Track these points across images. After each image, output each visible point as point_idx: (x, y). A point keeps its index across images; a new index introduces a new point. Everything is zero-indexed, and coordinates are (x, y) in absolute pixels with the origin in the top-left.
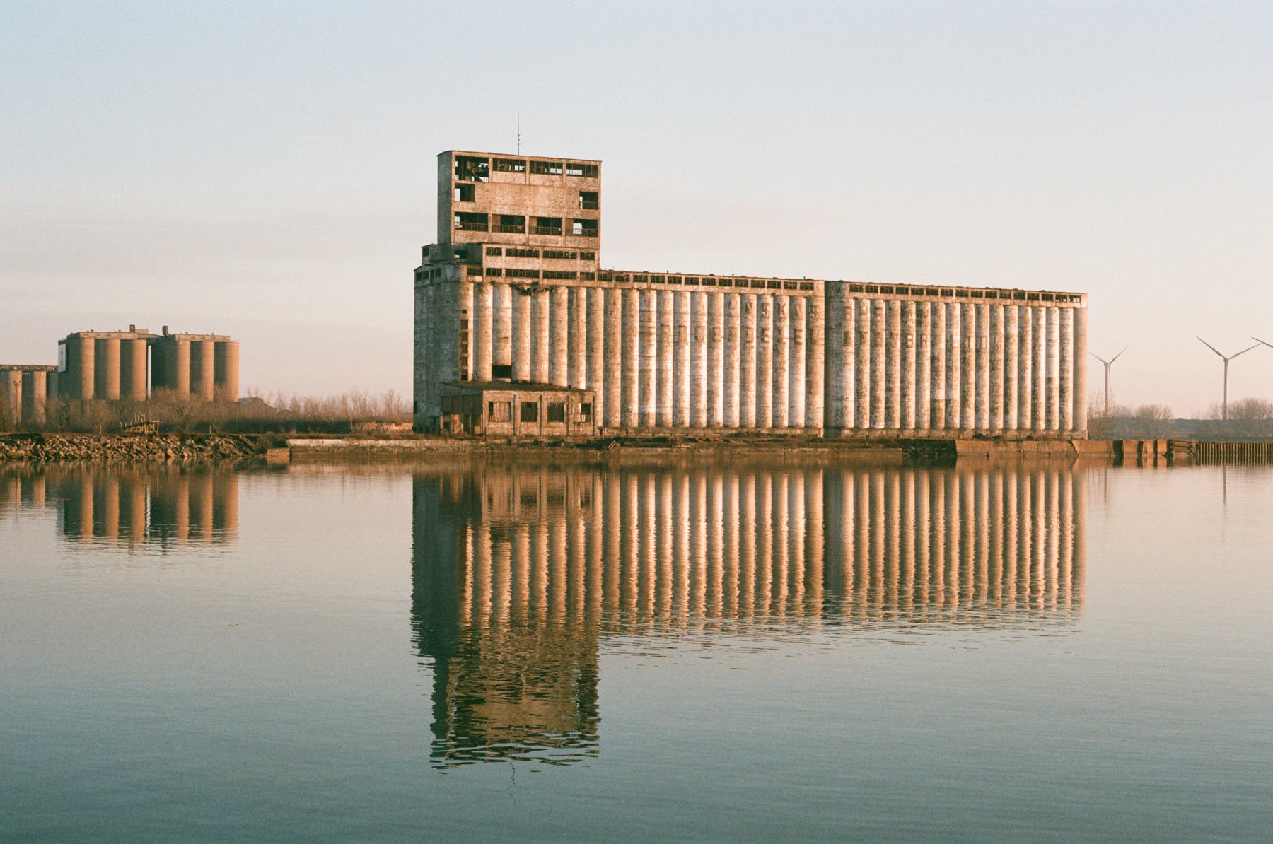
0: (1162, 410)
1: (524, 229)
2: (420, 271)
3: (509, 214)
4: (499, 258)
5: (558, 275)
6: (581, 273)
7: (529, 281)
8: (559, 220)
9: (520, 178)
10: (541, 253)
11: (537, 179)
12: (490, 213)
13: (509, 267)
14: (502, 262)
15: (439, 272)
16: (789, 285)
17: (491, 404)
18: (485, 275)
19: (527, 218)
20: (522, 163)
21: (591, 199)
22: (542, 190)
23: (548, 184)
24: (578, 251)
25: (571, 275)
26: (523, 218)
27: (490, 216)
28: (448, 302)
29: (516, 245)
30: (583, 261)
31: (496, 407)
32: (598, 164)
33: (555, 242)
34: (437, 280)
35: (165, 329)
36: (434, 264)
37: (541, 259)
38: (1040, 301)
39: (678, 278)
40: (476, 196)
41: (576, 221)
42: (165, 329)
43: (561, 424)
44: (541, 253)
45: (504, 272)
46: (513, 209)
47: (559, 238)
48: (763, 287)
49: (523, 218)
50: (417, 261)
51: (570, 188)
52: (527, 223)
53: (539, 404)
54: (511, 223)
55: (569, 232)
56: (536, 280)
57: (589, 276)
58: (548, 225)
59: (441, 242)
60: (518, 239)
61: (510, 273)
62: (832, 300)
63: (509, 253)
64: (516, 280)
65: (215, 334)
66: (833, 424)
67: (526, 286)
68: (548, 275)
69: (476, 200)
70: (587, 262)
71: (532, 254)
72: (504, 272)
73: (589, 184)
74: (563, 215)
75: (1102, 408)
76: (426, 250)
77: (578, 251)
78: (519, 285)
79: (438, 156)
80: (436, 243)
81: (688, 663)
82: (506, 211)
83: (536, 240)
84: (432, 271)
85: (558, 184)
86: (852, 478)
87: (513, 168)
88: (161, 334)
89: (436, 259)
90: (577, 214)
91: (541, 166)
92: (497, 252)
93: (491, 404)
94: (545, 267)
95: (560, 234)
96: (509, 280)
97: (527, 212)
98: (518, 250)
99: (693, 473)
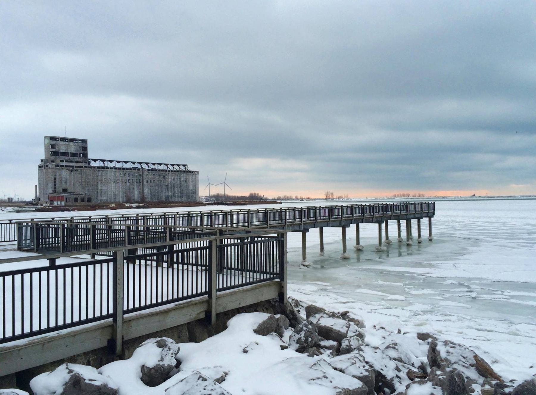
0: (287, 196)
2: (40, 165)
4: (63, 163)
6: (84, 166)
7: (71, 168)
8: (77, 153)
9: (67, 143)
10: (74, 162)
11: (71, 143)
12: (60, 152)
13: (66, 165)
14: (64, 164)
15: (47, 166)
17: (66, 198)
18: (60, 167)
19: (69, 153)
20: (68, 139)
22: (73, 146)
23: (74, 145)
24: (83, 161)
25: (82, 167)
26: (68, 153)
31: (68, 199)
33: (77, 159)
37: (74, 163)
41: (81, 154)
43: (84, 202)
44: (74, 162)
45: (65, 166)
47: (78, 158)
48: (128, 170)
49: (68, 153)
50: (40, 163)
51: (80, 146)
52: (69, 154)
54: (64, 154)
55: (80, 156)
56: (73, 168)
57: (86, 167)
58: (74, 155)
59: (46, 159)
60: (67, 158)
61: (66, 166)
63: (66, 161)
64: (68, 168)
65: (325, 194)
67: (71, 169)
68: (76, 167)
70: (85, 164)
71: (72, 162)
72: (65, 166)
73: (84, 145)
74: (78, 153)
75: (224, 193)
76: (42, 161)
77: (83, 161)
79: (95, 162)
80: (306, 233)
82: (63, 151)
83: (72, 158)
84: (45, 166)
85: (77, 145)
86: (117, 351)
87: (66, 141)
90: (82, 152)
91: (72, 140)
93: (66, 198)
94: (75, 165)
95: (77, 157)
97: (69, 151)
99: (55, 247)
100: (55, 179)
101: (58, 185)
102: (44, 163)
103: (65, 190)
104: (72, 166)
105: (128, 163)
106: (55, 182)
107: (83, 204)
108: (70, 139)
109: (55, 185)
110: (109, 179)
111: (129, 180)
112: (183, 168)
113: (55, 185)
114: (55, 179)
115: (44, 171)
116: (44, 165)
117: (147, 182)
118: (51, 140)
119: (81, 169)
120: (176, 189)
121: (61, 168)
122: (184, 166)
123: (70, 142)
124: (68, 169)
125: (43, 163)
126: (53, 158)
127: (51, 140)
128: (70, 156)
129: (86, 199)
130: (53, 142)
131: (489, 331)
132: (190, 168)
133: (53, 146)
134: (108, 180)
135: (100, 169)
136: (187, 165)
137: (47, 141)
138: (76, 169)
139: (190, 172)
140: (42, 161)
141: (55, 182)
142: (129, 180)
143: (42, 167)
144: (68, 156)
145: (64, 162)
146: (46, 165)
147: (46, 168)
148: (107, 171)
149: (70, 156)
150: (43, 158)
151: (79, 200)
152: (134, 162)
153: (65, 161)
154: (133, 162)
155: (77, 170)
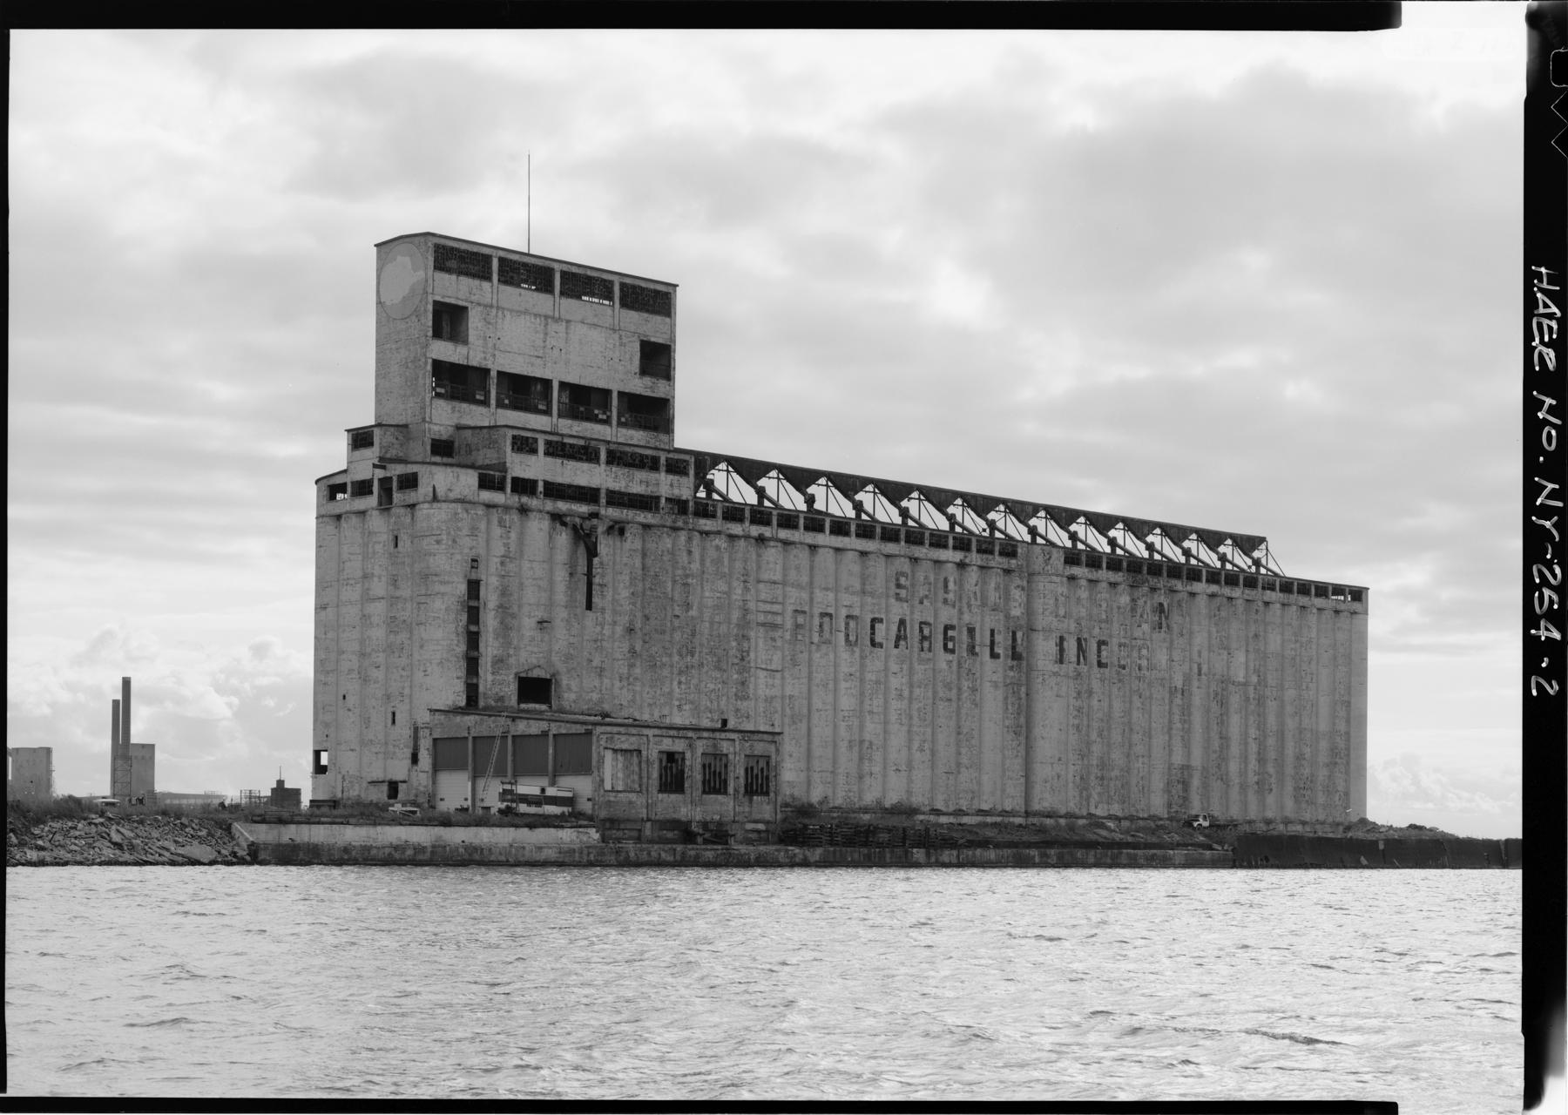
1: (609, 418)
3: (526, 374)
4: (533, 458)
5: (630, 500)
7: (584, 509)
13: (549, 478)
14: (537, 467)
16: (984, 547)
21: (657, 358)
25: (645, 503)
27: (493, 374)
28: (438, 542)
29: (562, 435)
30: (671, 477)
32: (670, 290)
36: (388, 466)
38: (1313, 598)
39: (819, 520)
40: (471, 332)
45: (541, 488)
46: (532, 365)
50: (335, 456)
53: (688, 755)
57: (680, 506)
59: (1361, 616)
61: (555, 491)
62: (1036, 578)
64: (562, 506)
66: (719, 725)
69: (471, 339)
71: (585, 453)
76: (360, 439)
78: (565, 515)
81: (1145, 1018)
89: (388, 456)
96: (549, 505)
97: (556, 373)
98: (564, 444)
100: (474, 587)
101: (489, 648)
102: (382, 463)
103: (535, 689)
104: (588, 495)
106: (474, 615)
108: (564, 274)
109: (473, 640)
110: (823, 615)
111: (950, 633)
112: (1242, 561)
113: (473, 640)
114: (474, 587)
115: (377, 522)
116: (380, 473)
118: (440, 266)
120: (1235, 721)
121: (514, 500)
122: (1248, 544)
123: (562, 293)
124: (557, 518)
125: (371, 454)
126: (445, 417)
127: (440, 266)
128: (560, 416)
129: (736, 776)
130: (454, 288)
131: (1051, 940)
133: (448, 320)
134: (816, 621)
135: (767, 532)
136: (1262, 540)
137: (414, 272)
138: (613, 513)
139: (1288, 586)
140: (360, 439)
141: (474, 615)
142: (950, 633)
143: (363, 488)
144: (548, 412)
145: (534, 451)
146: (396, 470)
147: (397, 497)
149: (560, 416)
150: (366, 418)
152: (985, 498)
153: (541, 448)
154: (975, 496)
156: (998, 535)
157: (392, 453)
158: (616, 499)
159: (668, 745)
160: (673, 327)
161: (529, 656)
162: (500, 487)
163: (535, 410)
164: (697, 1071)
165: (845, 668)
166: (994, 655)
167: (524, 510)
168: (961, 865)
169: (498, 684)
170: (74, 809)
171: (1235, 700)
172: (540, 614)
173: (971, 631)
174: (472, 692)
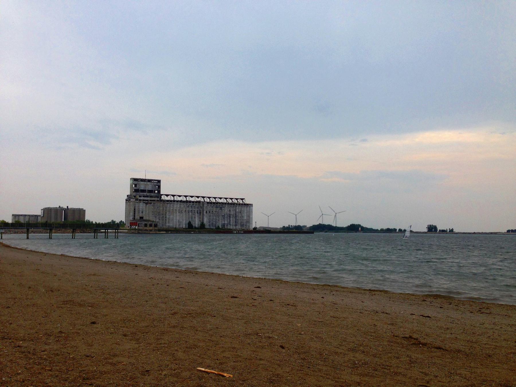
14: (142, 198)
17: (139, 224)
31: (140, 224)
33: (152, 194)
34: (130, 201)
35: (67, 207)
37: (149, 198)
42: (67, 207)
50: (126, 197)
57: (158, 201)
60: (145, 194)
61: (143, 200)
64: (145, 201)
67: (147, 203)
71: (147, 197)
76: (128, 196)
83: (148, 194)
88: (66, 208)
92: (140, 196)
93: (139, 224)
97: (147, 189)
100: (135, 209)
101: (136, 215)
104: (148, 200)
105: (194, 198)
106: (135, 212)
107: (151, 228)
109: (135, 214)
113: (135, 214)
114: (135, 209)
117: (206, 213)
119: (154, 202)
122: (242, 199)
124: (144, 203)
130: (136, 182)
132: (247, 201)
136: (244, 199)
140: (128, 196)
141: (135, 212)
145: (141, 197)
148: (174, 204)
151: (148, 226)
155: (151, 203)
156: (233, 202)
157: (130, 197)
158: (150, 200)
159: (145, 223)
160: (160, 184)
161: (141, 215)
162: (138, 200)
163: (145, 192)
164: (504, 235)
165: (178, 215)
166: (197, 213)
167: (140, 202)
168: (179, 233)
169: (137, 217)
170: (195, 228)
171: (232, 216)
172: (142, 211)
173: (194, 211)
174: (134, 218)
